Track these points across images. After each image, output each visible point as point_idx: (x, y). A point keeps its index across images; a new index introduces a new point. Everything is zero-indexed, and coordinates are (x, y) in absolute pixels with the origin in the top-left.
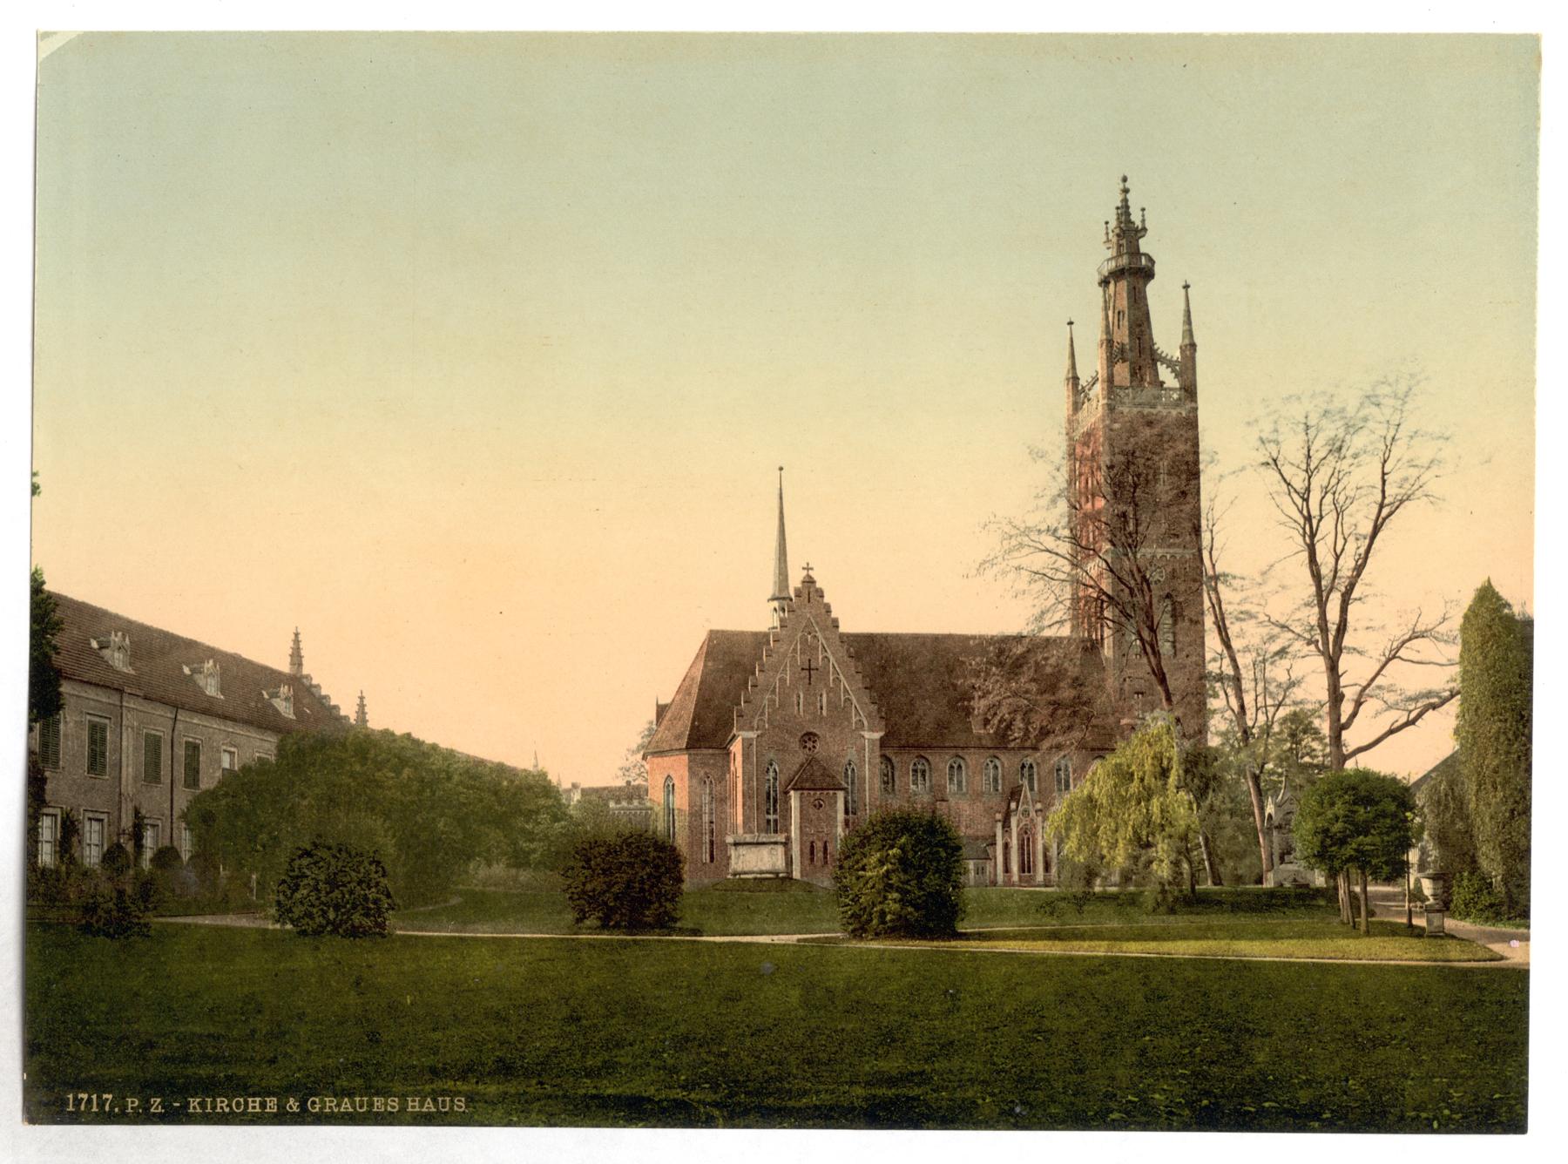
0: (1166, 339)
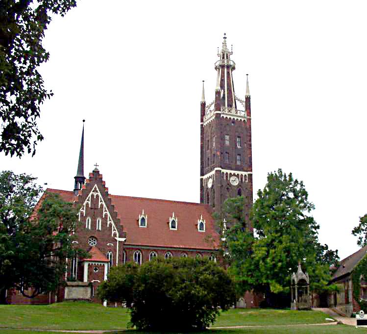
0: (240, 93)
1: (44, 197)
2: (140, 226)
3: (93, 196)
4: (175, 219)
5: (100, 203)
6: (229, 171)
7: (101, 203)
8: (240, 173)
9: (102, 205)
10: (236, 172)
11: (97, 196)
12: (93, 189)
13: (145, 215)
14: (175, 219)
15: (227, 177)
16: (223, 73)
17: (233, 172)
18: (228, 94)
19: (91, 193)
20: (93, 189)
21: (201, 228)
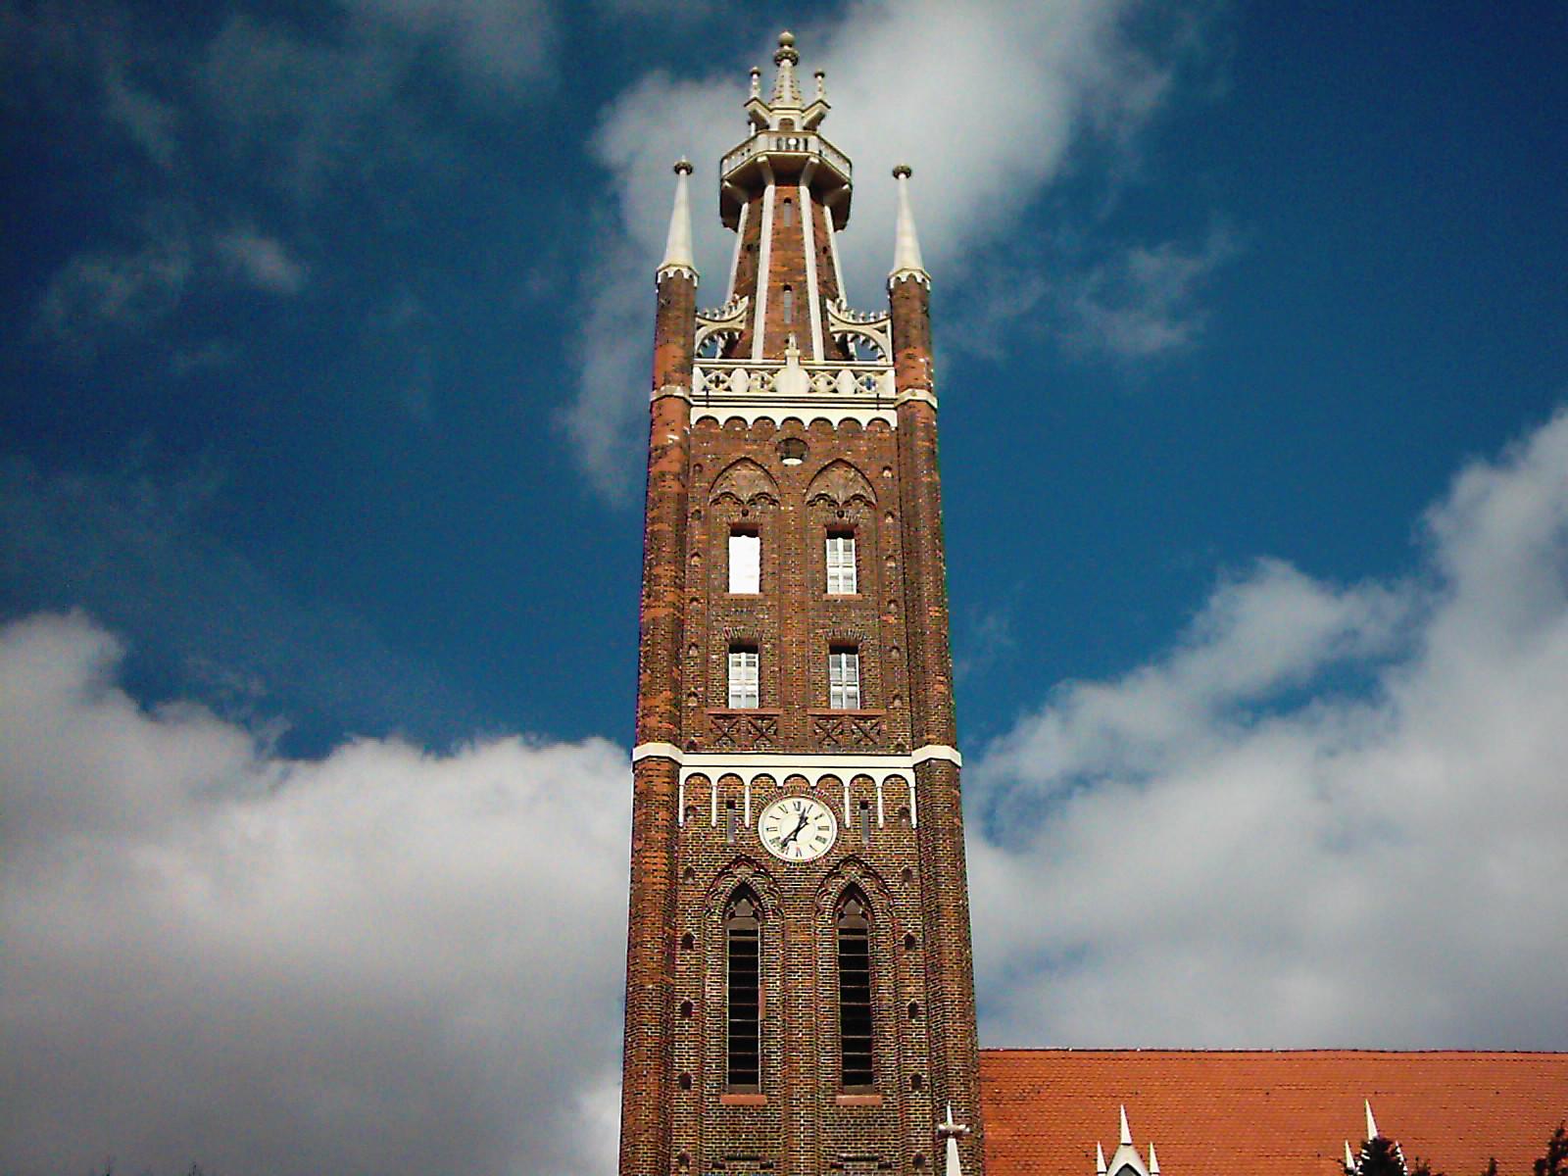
6: (748, 766)
8: (846, 767)
10: (813, 767)
17: (781, 766)
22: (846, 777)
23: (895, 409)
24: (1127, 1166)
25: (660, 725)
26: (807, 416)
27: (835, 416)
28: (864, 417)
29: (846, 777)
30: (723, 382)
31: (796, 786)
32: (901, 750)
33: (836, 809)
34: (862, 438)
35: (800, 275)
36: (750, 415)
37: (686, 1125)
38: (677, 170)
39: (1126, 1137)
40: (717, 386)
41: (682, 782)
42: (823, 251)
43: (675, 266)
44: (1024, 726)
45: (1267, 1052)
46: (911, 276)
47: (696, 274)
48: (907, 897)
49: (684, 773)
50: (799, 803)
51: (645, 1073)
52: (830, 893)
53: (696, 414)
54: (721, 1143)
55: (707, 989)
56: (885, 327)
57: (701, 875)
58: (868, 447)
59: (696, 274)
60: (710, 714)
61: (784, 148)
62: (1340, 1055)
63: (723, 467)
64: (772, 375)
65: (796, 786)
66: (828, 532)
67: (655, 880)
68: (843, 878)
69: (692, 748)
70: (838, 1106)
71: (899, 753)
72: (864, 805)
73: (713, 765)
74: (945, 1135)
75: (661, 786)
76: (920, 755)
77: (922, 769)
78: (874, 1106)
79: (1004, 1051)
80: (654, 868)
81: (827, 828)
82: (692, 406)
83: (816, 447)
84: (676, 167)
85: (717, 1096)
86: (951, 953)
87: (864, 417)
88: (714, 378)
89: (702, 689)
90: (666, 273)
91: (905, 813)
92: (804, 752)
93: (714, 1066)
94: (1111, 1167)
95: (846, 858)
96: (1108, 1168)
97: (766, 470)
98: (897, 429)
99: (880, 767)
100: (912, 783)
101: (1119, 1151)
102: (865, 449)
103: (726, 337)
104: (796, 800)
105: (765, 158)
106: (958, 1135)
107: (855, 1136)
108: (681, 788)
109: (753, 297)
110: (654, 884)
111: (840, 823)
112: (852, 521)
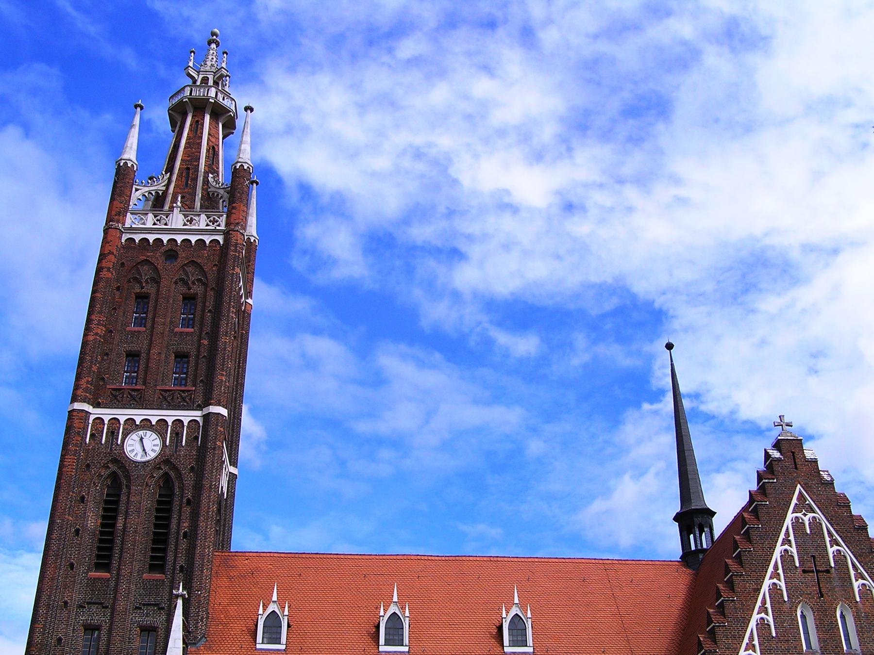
1: (767, 567)
2: (507, 650)
3: (798, 525)
4: (403, 608)
5: (831, 550)
6: (123, 415)
7: (786, 547)
8: (170, 416)
9: (840, 558)
10: (154, 415)
11: (815, 523)
12: (794, 501)
13: (522, 606)
14: (403, 608)
15: (113, 433)
16: (207, 94)
17: (139, 415)
18: (207, 157)
19: (790, 516)
20: (794, 501)
21: (273, 634)
22: (170, 421)
23: (224, 234)
24: (517, 614)
25: (82, 394)
26: (179, 238)
27: (193, 239)
28: (208, 239)
29: (170, 421)
30: (217, 221)
31: (146, 424)
32: (200, 408)
33: (163, 437)
34: (205, 250)
35: (196, 162)
36: (151, 238)
37: (69, 587)
38: (136, 106)
39: (275, 598)
40: (213, 224)
41: (91, 421)
42: (213, 152)
43: (124, 160)
44: (642, 405)
45: (573, 559)
46: (242, 166)
47: (251, 166)
48: (189, 480)
49: (92, 418)
50: (138, 434)
51: (50, 562)
52: (154, 477)
53: (124, 238)
54: (85, 596)
55: (89, 522)
56: (136, 188)
57: (93, 467)
58: (207, 254)
59: (251, 166)
60: (110, 388)
61: (206, 95)
62: (640, 562)
63: (135, 264)
64: (219, 218)
65: (146, 424)
66: (183, 297)
67: (68, 470)
68: (162, 470)
69: (97, 405)
70: (144, 580)
71: (198, 409)
72: (177, 434)
73: (106, 414)
74: (177, 596)
75: (76, 423)
76: (206, 411)
77: (206, 417)
78: (102, 579)
79: (647, 561)
80: (69, 464)
81: (157, 445)
82: (123, 232)
83: (182, 254)
84: (246, 107)
85: (87, 573)
86: (205, 508)
87: (208, 239)
88: (212, 219)
89: (108, 376)
90: (235, 167)
91: (196, 438)
92: (152, 408)
93: (87, 559)
94: (265, 613)
95: (164, 460)
96: (263, 613)
97: (155, 266)
98: (223, 245)
99: (187, 416)
100: (201, 425)
101: (270, 604)
102: (206, 255)
103: (154, 194)
104: (144, 431)
105: (213, 101)
106: (183, 596)
107: (85, 596)
108: (90, 425)
109: (171, 175)
110: (68, 471)
111: (164, 442)
112: (195, 291)
